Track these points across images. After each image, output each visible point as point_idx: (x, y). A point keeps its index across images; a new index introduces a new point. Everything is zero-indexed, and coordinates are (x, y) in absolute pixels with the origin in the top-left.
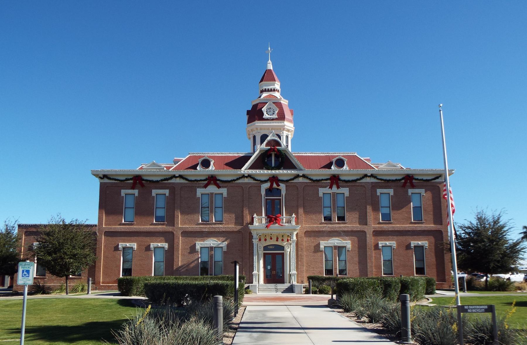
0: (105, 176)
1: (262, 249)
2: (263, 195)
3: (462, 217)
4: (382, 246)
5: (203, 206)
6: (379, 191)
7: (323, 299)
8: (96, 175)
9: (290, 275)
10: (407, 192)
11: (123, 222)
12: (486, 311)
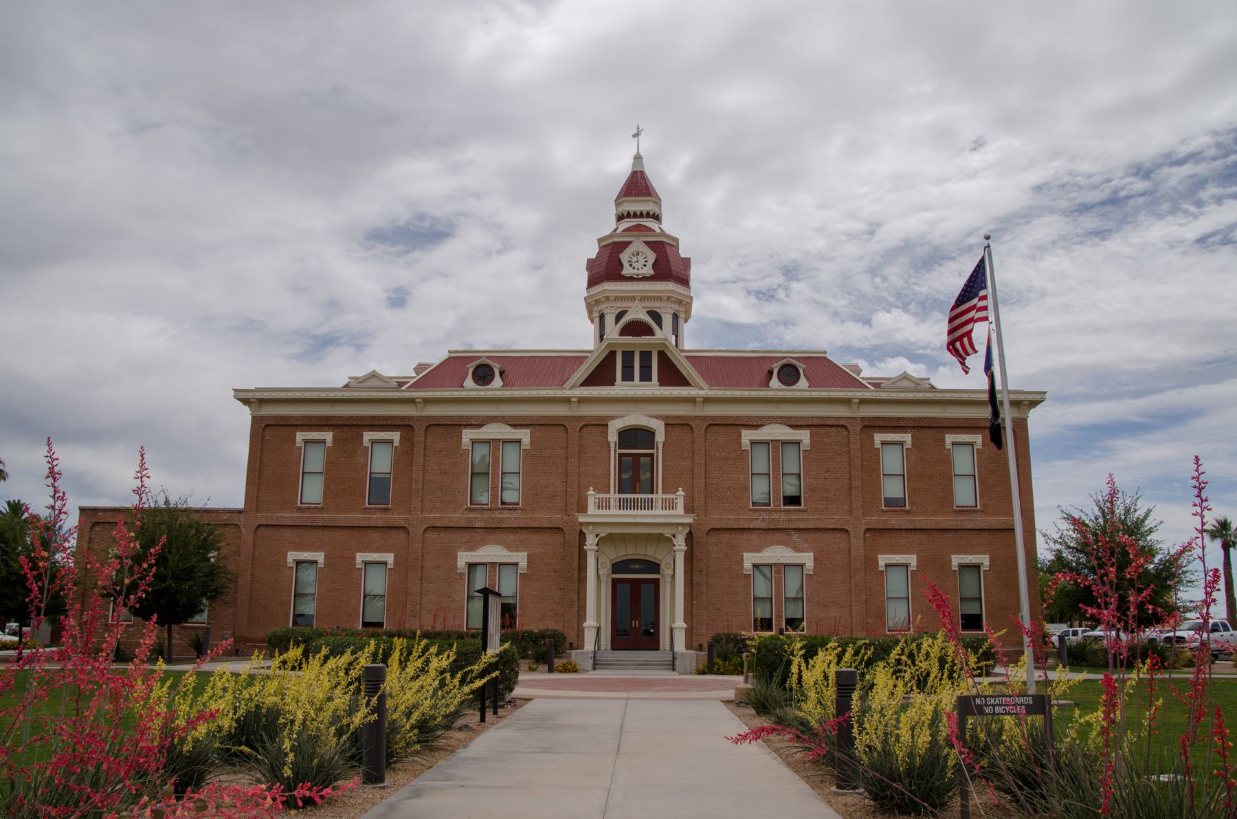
0: (262, 402)
1: (609, 566)
2: (612, 446)
3: (1059, 503)
4: (887, 565)
5: (476, 470)
6: (879, 438)
7: (725, 686)
8: (246, 401)
9: (672, 630)
10: (944, 440)
11: (313, 491)
12: (1030, 710)
